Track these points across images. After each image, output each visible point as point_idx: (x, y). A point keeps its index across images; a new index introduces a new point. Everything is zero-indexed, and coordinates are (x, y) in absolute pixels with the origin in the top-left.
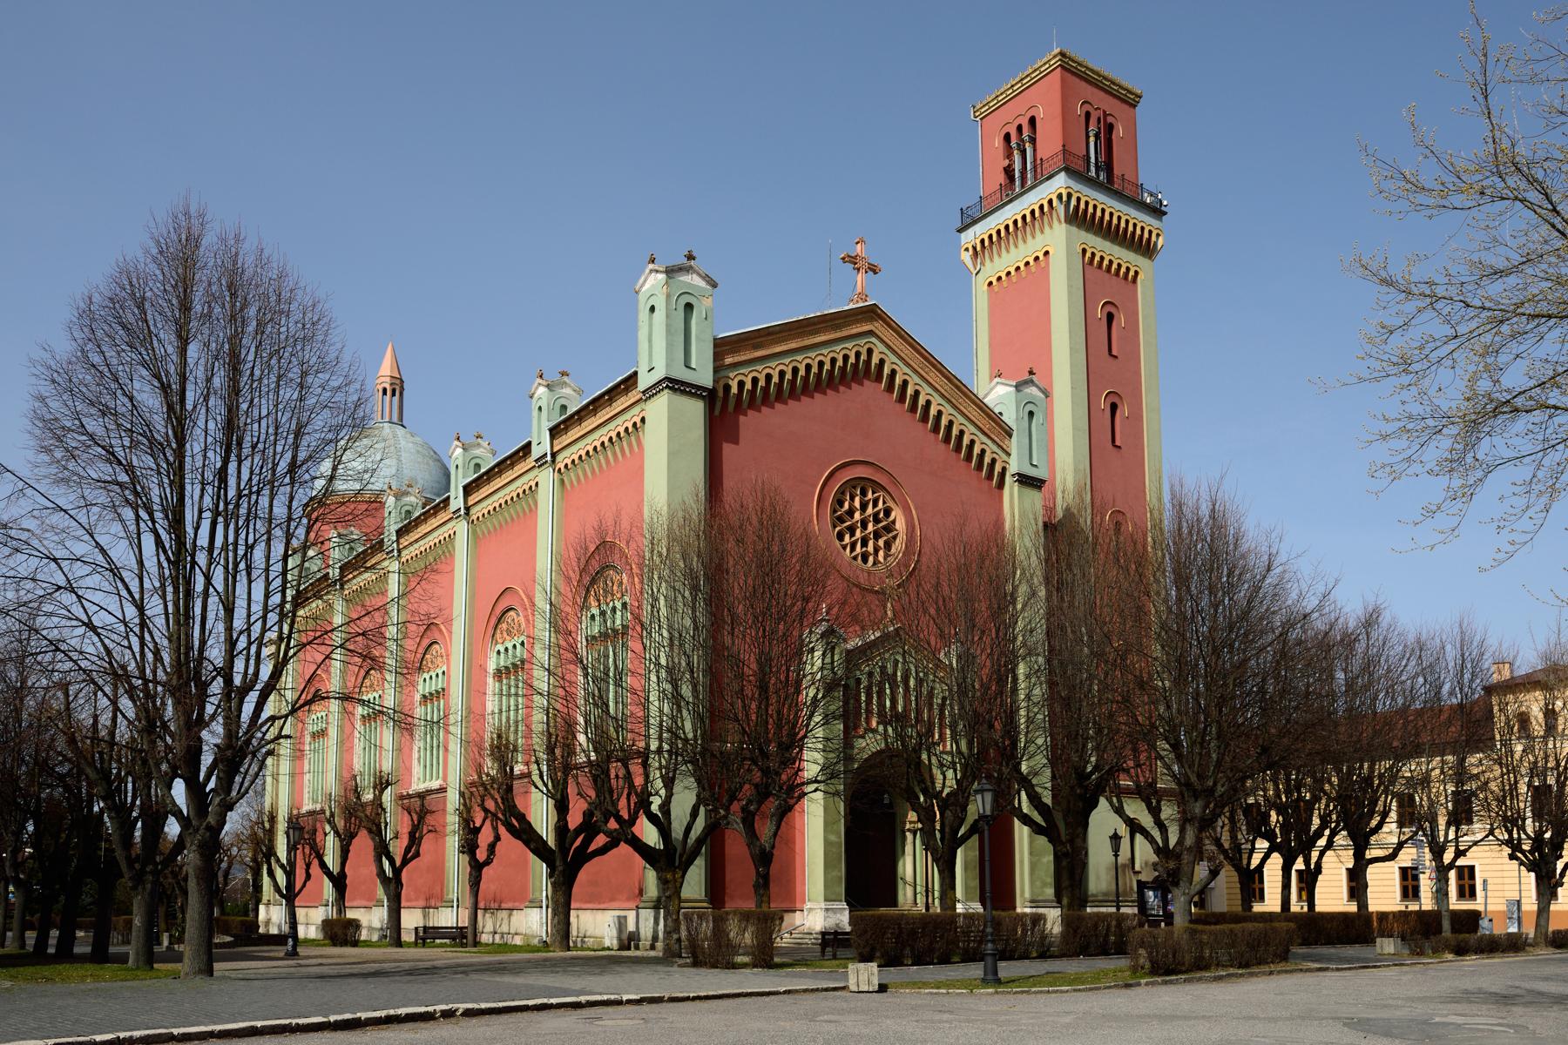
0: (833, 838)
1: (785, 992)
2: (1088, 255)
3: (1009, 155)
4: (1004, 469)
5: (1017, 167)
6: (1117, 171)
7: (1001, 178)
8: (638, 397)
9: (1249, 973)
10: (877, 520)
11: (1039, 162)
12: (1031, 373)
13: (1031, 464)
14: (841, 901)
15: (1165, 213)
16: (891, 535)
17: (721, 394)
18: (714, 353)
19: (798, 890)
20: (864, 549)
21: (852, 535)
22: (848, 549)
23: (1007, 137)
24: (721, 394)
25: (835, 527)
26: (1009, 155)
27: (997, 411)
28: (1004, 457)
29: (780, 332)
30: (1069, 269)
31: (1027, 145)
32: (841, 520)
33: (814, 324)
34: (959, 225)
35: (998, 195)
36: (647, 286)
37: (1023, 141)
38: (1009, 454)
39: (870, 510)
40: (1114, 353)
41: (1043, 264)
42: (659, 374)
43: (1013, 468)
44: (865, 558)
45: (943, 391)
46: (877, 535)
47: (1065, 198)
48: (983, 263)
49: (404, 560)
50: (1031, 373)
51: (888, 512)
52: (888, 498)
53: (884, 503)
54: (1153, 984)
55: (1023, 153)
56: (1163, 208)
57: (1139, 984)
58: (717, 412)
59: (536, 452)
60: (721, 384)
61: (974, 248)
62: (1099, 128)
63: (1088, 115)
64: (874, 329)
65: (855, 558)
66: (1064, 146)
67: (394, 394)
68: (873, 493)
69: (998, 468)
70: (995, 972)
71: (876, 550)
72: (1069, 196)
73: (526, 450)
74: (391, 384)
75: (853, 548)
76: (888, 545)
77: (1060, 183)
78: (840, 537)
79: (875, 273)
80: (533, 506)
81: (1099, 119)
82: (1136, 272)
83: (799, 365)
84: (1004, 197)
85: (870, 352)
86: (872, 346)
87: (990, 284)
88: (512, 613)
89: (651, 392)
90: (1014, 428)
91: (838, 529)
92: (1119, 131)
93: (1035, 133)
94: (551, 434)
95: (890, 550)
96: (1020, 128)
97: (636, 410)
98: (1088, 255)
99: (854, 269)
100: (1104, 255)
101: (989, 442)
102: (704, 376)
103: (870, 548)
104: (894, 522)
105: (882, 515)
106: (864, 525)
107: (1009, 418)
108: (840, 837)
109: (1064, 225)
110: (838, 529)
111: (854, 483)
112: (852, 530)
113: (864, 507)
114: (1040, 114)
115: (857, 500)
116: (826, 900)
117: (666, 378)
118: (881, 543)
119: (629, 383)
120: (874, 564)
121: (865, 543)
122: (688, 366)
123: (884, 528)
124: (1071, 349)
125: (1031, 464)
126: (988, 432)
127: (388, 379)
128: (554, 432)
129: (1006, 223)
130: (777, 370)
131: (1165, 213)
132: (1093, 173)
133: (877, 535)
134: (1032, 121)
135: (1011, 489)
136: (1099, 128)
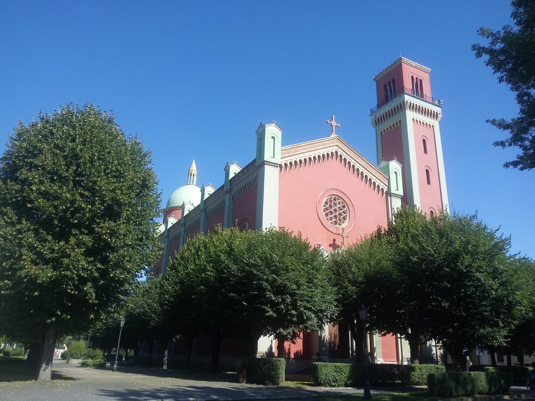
3: (386, 90)
22: (329, 219)
23: (385, 86)
25: (346, 216)
32: (327, 209)
41: (399, 124)
46: (340, 214)
49: (186, 226)
55: (391, 90)
61: (376, 121)
64: (338, 145)
80: (200, 222)
85: (336, 152)
87: (381, 132)
93: (395, 84)
96: (389, 83)
113: (335, 204)
115: (332, 202)
119: (254, 163)
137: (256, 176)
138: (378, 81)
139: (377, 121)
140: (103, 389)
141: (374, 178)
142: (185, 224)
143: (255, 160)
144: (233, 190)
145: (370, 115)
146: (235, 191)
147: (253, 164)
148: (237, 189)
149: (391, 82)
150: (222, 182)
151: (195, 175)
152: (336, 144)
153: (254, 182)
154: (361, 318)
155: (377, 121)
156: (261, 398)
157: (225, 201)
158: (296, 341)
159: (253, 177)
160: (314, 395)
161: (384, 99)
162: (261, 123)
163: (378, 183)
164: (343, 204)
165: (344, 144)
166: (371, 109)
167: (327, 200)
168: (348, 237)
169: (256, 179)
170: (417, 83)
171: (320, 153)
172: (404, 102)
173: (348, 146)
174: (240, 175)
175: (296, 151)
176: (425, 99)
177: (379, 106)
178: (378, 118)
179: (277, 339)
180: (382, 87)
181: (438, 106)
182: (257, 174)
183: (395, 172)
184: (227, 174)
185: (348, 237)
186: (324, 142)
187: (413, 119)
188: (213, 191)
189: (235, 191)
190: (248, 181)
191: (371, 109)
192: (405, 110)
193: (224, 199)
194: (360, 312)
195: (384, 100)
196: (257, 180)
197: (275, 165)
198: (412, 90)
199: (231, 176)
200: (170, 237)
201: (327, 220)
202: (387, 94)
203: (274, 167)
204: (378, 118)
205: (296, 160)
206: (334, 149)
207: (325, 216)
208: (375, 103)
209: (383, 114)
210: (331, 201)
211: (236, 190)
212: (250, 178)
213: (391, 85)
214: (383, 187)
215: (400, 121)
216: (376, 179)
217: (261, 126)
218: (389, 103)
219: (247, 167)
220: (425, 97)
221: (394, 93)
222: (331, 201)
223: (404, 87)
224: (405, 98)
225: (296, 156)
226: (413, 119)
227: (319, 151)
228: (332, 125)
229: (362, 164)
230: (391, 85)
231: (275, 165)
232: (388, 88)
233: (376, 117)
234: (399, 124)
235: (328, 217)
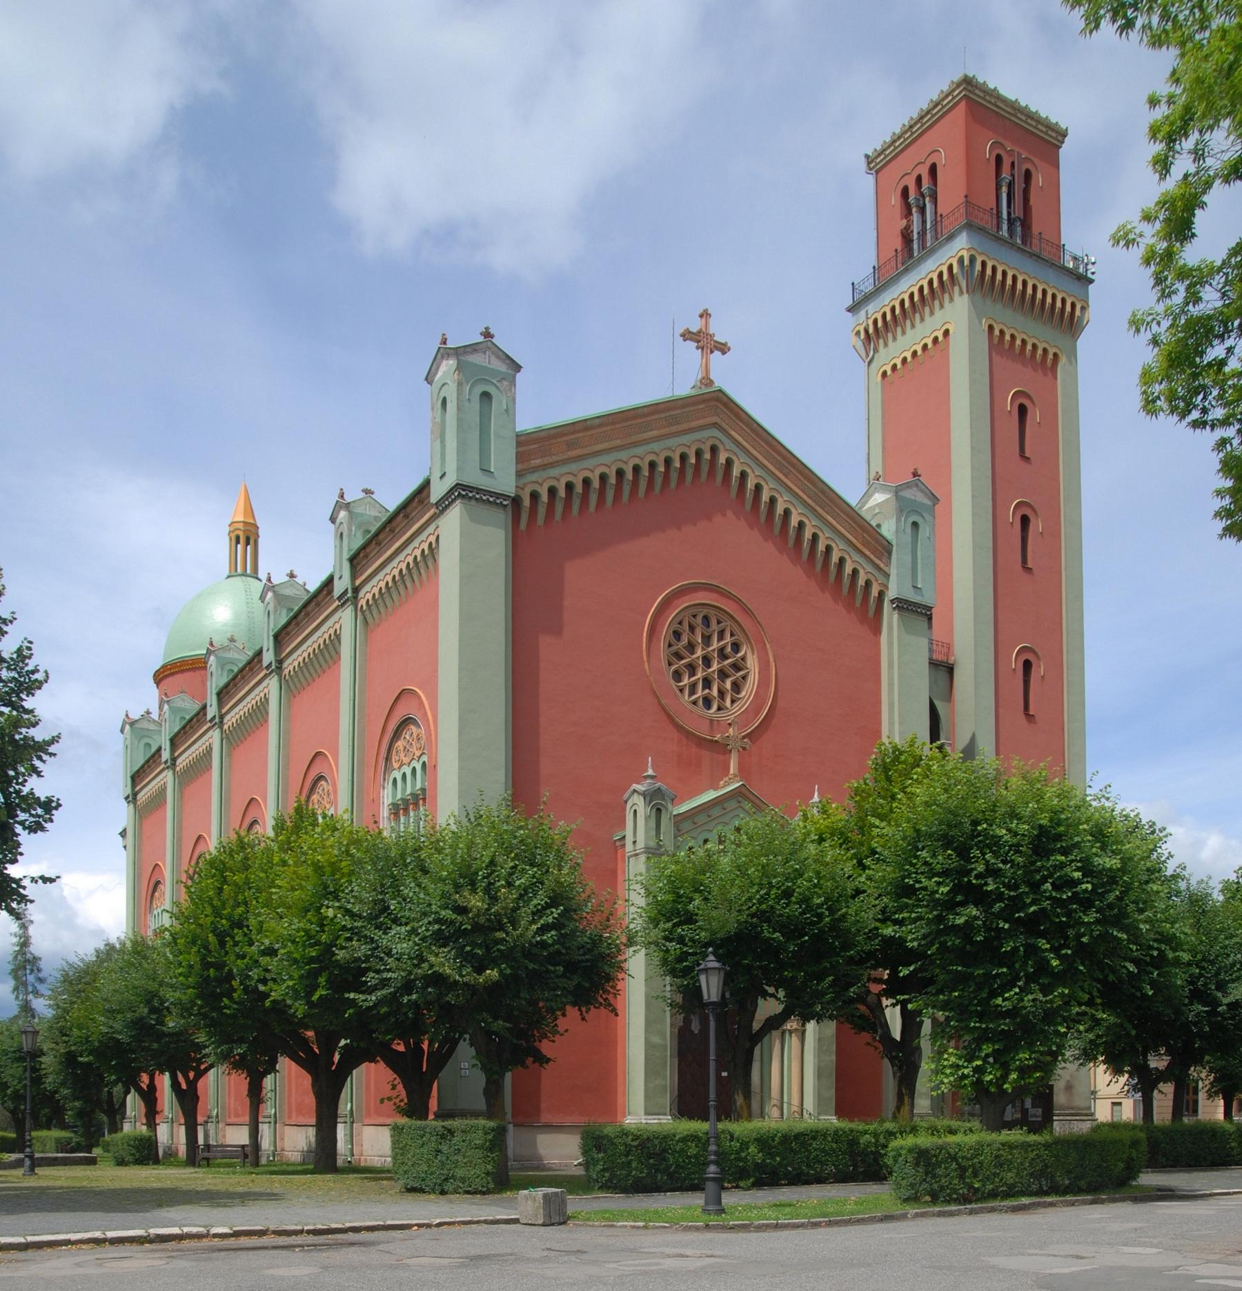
0: (656, 1040)
1: (439, 1225)
2: (997, 333)
3: (908, 214)
4: (881, 594)
5: (916, 228)
6: (1035, 230)
7: (898, 243)
8: (433, 511)
9: (1061, 1202)
10: (723, 655)
11: (939, 219)
12: (915, 474)
13: (915, 587)
14: (665, 1114)
15: (1091, 281)
16: (741, 673)
17: (527, 502)
18: (517, 453)
19: (619, 1101)
20: (707, 691)
21: (693, 674)
22: (687, 692)
24: (527, 502)
25: (670, 664)
26: (908, 214)
27: (874, 524)
28: (881, 579)
29: (600, 426)
30: (971, 350)
31: (927, 199)
33: (644, 416)
34: (849, 302)
35: (893, 263)
36: (440, 374)
37: (923, 196)
38: (887, 576)
39: (715, 645)
40: (1027, 455)
42: (450, 481)
43: (892, 593)
44: (707, 702)
45: (805, 497)
46: (723, 674)
47: (966, 262)
48: (876, 350)
49: (226, 727)
50: (915, 474)
51: (736, 647)
52: (736, 629)
53: (732, 635)
54: (923, 1215)
55: (922, 210)
56: (1089, 275)
57: (903, 1217)
58: (523, 525)
59: (339, 587)
60: (528, 491)
61: (866, 331)
62: (1013, 176)
63: (999, 159)
65: (695, 703)
66: (966, 196)
67: (248, 543)
68: (719, 622)
69: (875, 592)
70: (719, 1202)
71: (722, 694)
72: (972, 259)
73: (330, 586)
74: (244, 531)
75: (692, 692)
76: (737, 687)
77: (961, 246)
78: (677, 676)
79: (724, 353)
81: (1013, 164)
82: (1055, 355)
83: (624, 467)
84: (899, 265)
85: (714, 450)
86: (717, 443)
87: (884, 374)
88: (323, 782)
89: (444, 505)
90: (894, 543)
91: (673, 668)
92: (1038, 180)
95: (738, 693)
97: (431, 529)
98: (997, 333)
99: (697, 348)
100: (1048, 347)
102: (505, 481)
103: (715, 692)
104: (743, 659)
105: (729, 649)
106: (707, 661)
107: (888, 530)
108: (665, 1039)
109: (966, 296)
110: (673, 668)
111: (694, 611)
112: (692, 669)
113: (707, 640)
114: (941, 159)
116: (647, 1113)
117: (457, 484)
118: (728, 684)
120: (719, 709)
121: (707, 683)
122: (486, 471)
123: (681, 658)
124: (973, 448)
125: (915, 587)
126: (861, 547)
127: (241, 526)
128: (355, 562)
129: (901, 297)
130: (597, 473)
131: (1091, 281)
132: (1004, 232)
133: (723, 674)
134: (933, 170)
135: (891, 618)
136: (1013, 176)
137: (432, 539)
138: (1151, 128)
139: (871, 330)
142: (222, 717)
144: (285, 665)
146: (369, 596)
152: (715, 419)
154: (705, 996)
159: (425, 546)
160: (1203, 1270)
161: (899, 249)
167: (680, 623)
168: (744, 749)
171: (658, 451)
175: (571, 446)
176: (1036, 250)
178: (875, 321)
179: (284, 1063)
180: (895, 200)
185: (744, 749)
186: (673, 413)
193: (337, 626)
194: (703, 978)
200: (181, 766)
201: (678, 692)
203: (473, 502)
204: (875, 321)
205: (570, 478)
207: (672, 682)
208: (869, 259)
209: (891, 304)
210: (692, 628)
214: (870, 577)
217: (442, 350)
222: (692, 628)
225: (573, 467)
227: (655, 446)
229: (801, 494)
232: (911, 199)
235: (680, 681)
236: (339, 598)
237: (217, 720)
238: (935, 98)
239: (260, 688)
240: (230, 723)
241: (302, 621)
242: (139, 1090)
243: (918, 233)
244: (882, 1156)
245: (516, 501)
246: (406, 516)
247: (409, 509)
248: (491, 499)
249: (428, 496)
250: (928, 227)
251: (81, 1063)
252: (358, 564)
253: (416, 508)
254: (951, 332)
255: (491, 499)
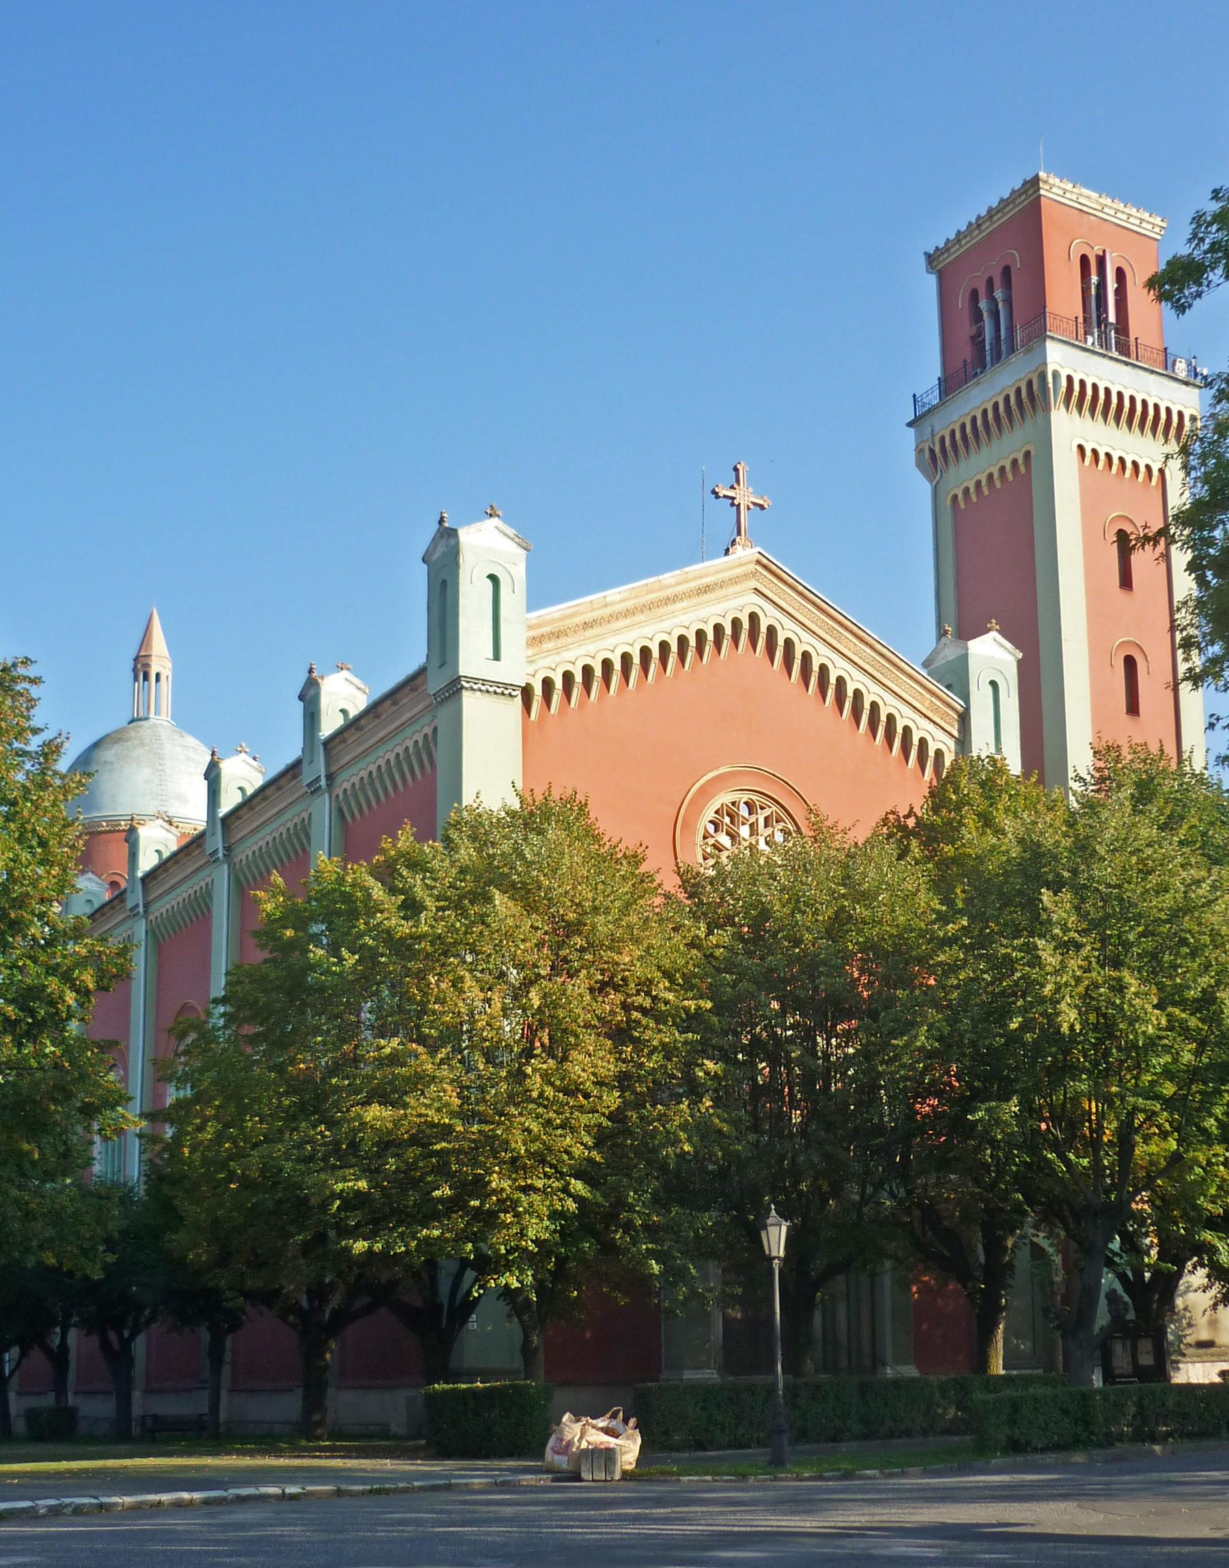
3: (977, 316)
23: (974, 296)
41: (1023, 470)
49: (152, 917)
59: (307, 776)
61: (932, 451)
63: (1084, 260)
73: (296, 770)
85: (753, 618)
87: (955, 497)
94: (325, 749)
96: (990, 282)
101: (931, 727)
119: (417, 682)
137: (428, 730)
139: (937, 450)
140: (1129, 1549)
141: (906, 711)
143: (422, 671)
144: (338, 780)
145: (910, 424)
146: (347, 785)
147: (416, 682)
148: (356, 780)
149: (997, 282)
150: (292, 750)
151: (163, 678)
153: (424, 756)
155: (937, 450)
156: (1028, 1372)
157: (309, 824)
158: (1192, 589)
162: (441, 520)
163: (921, 729)
164: (783, 824)
165: (785, 582)
166: (914, 396)
169: (432, 744)
170: (1102, 285)
172: (1043, 377)
173: (800, 588)
174: (363, 722)
177: (950, 384)
178: (943, 439)
181: (1186, 383)
182: (433, 725)
183: (993, 684)
184: (312, 717)
187: (1081, 448)
188: (258, 781)
189: (347, 785)
190: (400, 750)
191: (914, 396)
192: (1047, 409)
195: (965, 361)
196: (433, 749)
197: (502, 690)
198: (1081, 320)
199: (330, 724)
202: (980, 332)
203: (478, 693)
204: (943, 439)
206: (752, 603)
209: (962, 421)
211: (362, 778)
212: (407, 740)
213: (998, 294)
215: (1027, 455)
216: (916, 717)
218: (985, 378)
219: (392, 696)
220: (1133, 348)
221: (1007, 329)
223: (1047, 310)
224: (1049, 360)
226: (1081, 448)
228: (736, 502)
230: (998, 294)
231: (502, 690)
232: (983, 305)
233: (933, 435)
234: (1023, 470)
236: (309, 785)
237: (141, 909)
238: (1006, 195)
239: (201, 875)
240: (158, 914)
241: (258, 804)
242: (48, 1351)
243: (991, 344)
244: (316, 923)
245: (527, 692)
246: (395, 703)
247: (398, 696)
248: (499, 691)
249: (425, 682)
250: (1003, 337)
251: (986, 1259)
252: (334, 748)
253: (408, 695)
254: (1033, 454)
255: (499, 691)
